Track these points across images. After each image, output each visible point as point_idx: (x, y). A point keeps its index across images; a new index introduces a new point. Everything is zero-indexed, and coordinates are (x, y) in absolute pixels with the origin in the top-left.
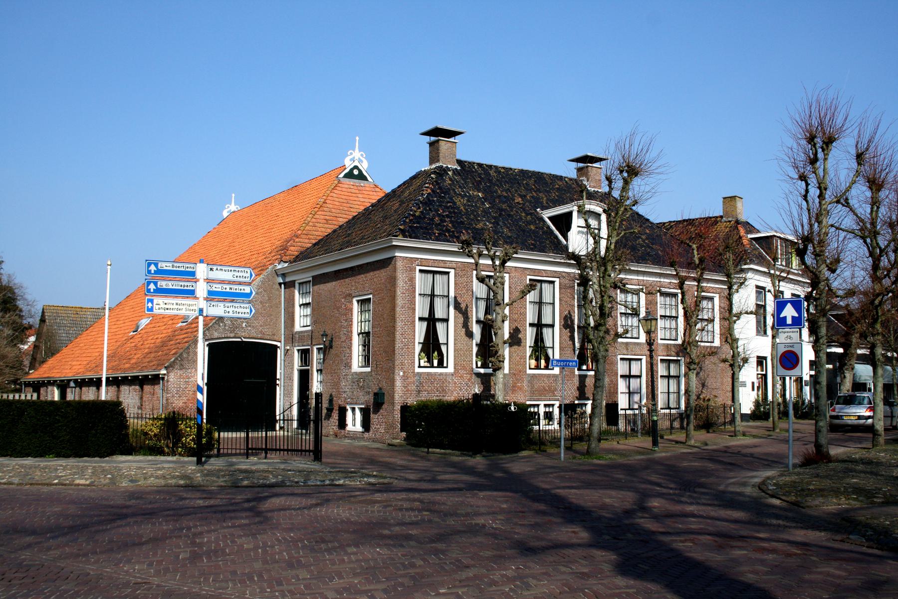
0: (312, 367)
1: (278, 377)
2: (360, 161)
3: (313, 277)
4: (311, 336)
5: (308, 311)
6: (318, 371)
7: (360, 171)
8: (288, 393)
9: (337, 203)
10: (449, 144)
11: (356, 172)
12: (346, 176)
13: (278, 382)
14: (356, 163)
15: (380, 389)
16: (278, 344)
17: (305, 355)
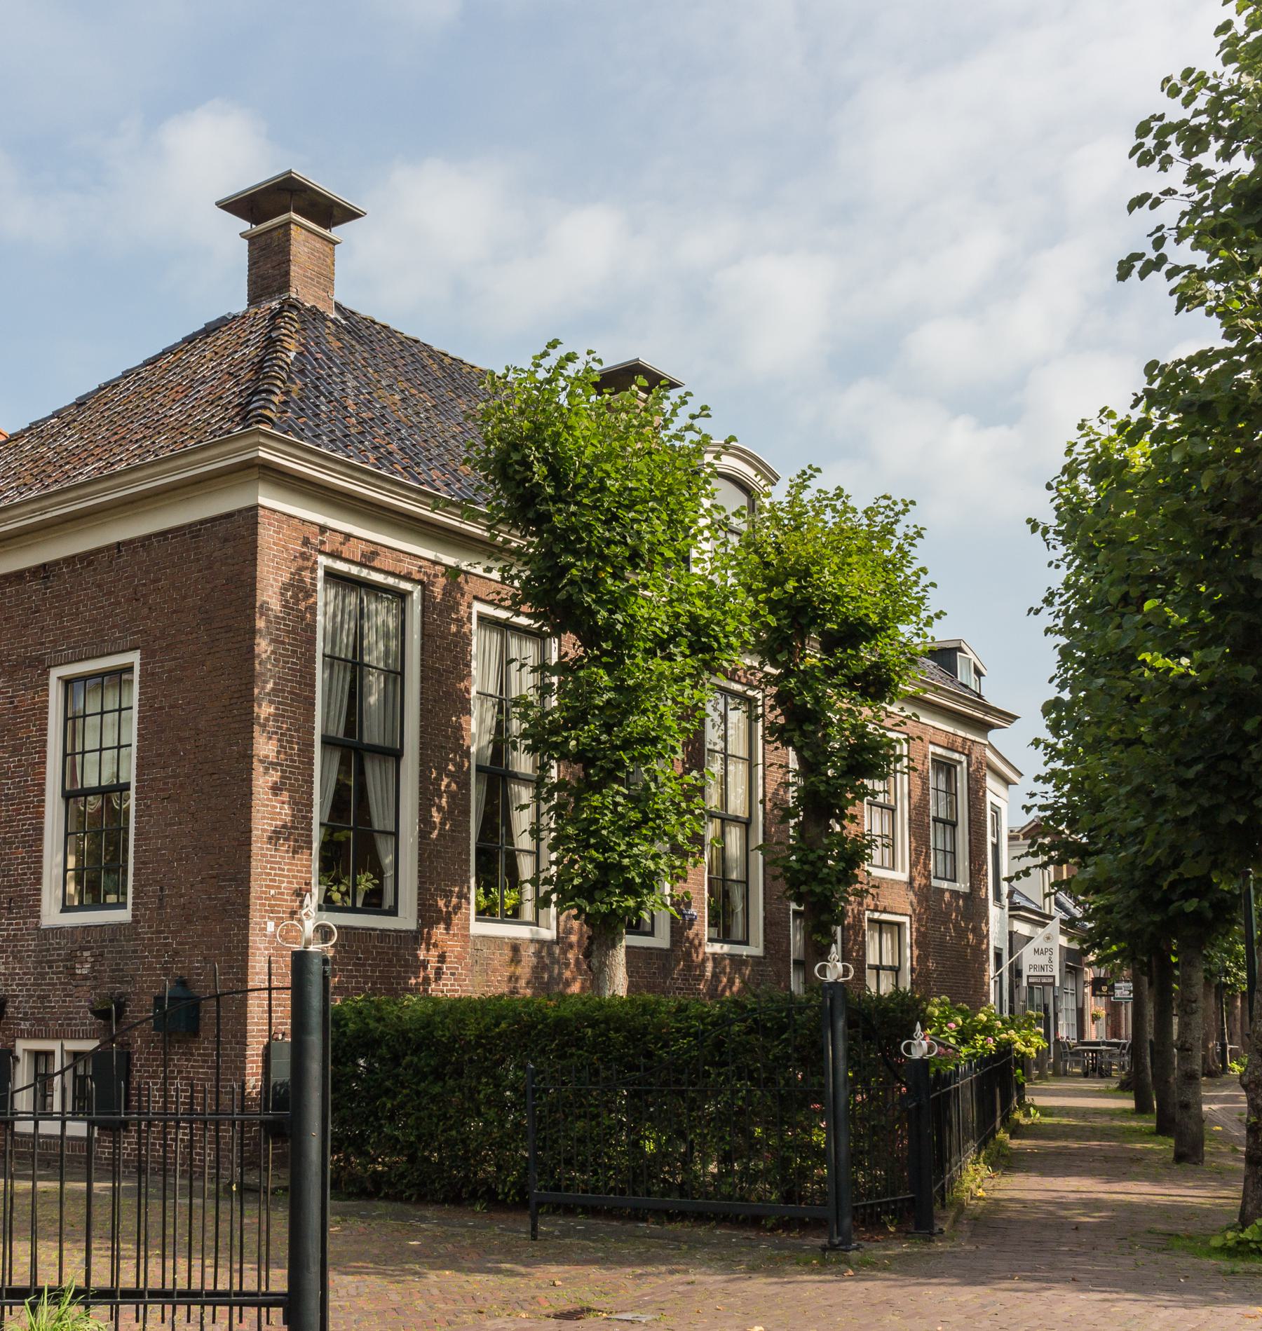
10: (318, 244)
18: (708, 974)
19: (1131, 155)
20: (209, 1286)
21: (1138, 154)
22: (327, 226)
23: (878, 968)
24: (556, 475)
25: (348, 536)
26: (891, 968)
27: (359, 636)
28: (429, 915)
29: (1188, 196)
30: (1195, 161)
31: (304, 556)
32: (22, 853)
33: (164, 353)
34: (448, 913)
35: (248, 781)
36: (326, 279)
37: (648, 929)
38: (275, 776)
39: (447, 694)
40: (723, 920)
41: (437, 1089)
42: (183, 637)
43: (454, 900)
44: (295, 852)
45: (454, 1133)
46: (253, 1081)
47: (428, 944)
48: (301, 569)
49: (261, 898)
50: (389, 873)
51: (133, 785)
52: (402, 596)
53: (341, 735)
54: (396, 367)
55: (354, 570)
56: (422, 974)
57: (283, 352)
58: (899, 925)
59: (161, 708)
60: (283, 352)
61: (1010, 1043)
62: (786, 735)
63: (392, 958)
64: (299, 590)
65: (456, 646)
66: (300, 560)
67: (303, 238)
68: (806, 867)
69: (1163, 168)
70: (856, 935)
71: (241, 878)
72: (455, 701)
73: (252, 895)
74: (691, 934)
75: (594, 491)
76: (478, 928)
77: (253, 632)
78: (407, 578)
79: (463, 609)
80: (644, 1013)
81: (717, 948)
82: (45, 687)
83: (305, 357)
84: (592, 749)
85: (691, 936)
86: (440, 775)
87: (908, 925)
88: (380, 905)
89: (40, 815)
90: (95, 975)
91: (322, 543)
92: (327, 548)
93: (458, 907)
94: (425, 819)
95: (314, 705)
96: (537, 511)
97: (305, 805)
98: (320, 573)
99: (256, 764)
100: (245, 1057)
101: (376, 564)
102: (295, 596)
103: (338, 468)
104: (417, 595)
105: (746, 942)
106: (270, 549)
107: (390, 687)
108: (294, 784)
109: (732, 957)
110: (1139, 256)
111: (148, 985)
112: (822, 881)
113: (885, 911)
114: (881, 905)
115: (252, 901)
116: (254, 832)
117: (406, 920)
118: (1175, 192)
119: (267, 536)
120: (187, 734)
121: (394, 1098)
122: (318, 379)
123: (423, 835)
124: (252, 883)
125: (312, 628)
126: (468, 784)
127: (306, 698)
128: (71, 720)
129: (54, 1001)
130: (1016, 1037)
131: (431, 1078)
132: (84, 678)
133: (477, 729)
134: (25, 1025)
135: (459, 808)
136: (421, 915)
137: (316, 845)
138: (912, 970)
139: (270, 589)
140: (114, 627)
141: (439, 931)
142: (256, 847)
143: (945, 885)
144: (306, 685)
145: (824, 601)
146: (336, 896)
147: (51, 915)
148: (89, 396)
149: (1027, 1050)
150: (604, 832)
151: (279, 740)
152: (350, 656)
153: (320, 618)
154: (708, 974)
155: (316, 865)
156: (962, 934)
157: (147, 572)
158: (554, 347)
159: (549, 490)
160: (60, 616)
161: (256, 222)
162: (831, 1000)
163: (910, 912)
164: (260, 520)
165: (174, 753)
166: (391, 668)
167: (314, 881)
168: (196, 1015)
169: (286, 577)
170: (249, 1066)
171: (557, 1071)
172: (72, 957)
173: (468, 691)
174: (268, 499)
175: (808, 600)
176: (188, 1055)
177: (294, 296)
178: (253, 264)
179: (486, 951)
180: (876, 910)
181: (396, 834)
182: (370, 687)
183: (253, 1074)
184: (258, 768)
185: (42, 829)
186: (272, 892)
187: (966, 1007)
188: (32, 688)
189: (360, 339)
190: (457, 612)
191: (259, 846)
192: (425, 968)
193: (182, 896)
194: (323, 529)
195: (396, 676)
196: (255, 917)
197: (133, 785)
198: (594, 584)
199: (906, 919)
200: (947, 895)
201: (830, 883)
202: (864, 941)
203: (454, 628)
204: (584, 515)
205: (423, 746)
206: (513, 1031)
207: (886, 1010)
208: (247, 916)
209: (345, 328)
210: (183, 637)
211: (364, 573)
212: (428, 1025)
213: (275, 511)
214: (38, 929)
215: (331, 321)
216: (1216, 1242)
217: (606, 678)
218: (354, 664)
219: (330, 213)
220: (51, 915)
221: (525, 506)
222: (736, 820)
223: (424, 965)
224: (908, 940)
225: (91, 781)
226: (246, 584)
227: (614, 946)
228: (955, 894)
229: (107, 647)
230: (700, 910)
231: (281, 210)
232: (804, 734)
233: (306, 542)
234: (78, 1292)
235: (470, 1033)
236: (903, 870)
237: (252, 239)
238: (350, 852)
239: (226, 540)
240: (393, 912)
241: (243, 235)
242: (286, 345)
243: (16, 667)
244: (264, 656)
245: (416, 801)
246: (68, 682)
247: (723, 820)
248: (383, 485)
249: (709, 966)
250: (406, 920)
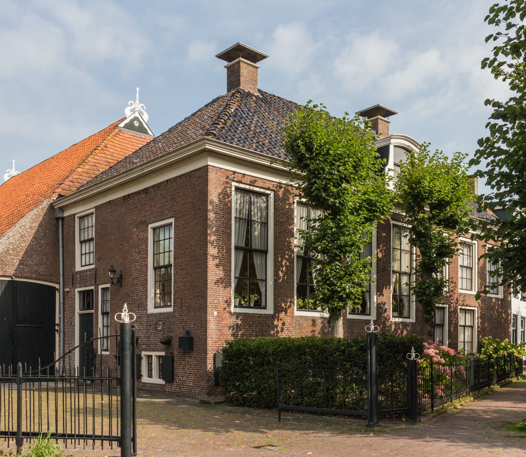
0: (97, 310)
1: (57, 322)
2: (140, 113)
3: (96, 207)
4: (95, 276)
5: (91, 247)
6: (103, 314)
7: (140, 123)
8: (68, 337)
9: (119, 149)
10: (251, 69)
11: (136, 124)
12: (126, 126)
13: (57, 328)
14: (137, 115)
15: (188, 333)
16: (57, 286)
17: (88, 299)
18: (393, 329)
19: (485, 20)
20: (77, 433)
21: (488, 20)
22: (255, 62)
23: (464, 326)
24: (309, 149)
25: (244, 175)
26: (470, 326)
27: (250, 210)
28: (278, 309)
29: (506, 35)
30: (508, 21)
31: (227, 183)
32: (141, 288)
33: (198, 111)
34: (286, 308)
35: (206, 263)
36: (255, 81)
37: (368, 313)
38: (217, 261)
39: (285, 230)
40: (398, 309)
41: (261, 370)
42: (187, 213)
43: (288, 304)
44: (225, 287)
45: (266, 385)
46: (210, 366)
47: (278, 319)
48: (225, 187)
49: (211, 303)
50: (263, 294)
51: (173, 264)
52: (267, 195)
53: (243, 246)
54: (278, 112)
55: (247, 187)
56: (276, 330)
57: (239, 109)
58: (473, 311)
59: (180, 238)
60: (239, 109)
61: (513, 353)
62: (414, 242)
63: (266, 324)
64: (225, 195)
65: (288, 213)
66: (225, 184)
67: (245, 67)
68: (421, 290)
69: (497, 24)
70: (455, 314)
71: (204, 297)
72: (287, 233)
73: (208, 302)
74: (386, 315)
75: (324, 155)
76: (297, 313)
77: (206, 210)
78: (268, 189)
79: (291, 200)
80: (325, 343)
81: (397, 320)
82: (147, 231)
83: (238, 110)
84: (327, 249)
85: (386, 316)
86: (282, 259)
87: (477, 311)
88: (261, 305)
89: (147, 275)
90: (163, 330)
91: (234, 178)
92: (236, 179)
93: (290, 306)
94: (276, 274)
95: (231, 235)
96: (304, 163)
97: (228, 271)
98: (233, 189)
99: (209, 256)
100: (206, 358)
101: (256, 184)
102: (224, 197)
103: (237, 150)
104: (272, 195)
105: (409, 318)
106: (213, 180)
107: (263, 229)
108: (224, 263)
109: (402, 323)
110: (488, 59)
111: (179, 333)
112: (427, 295)
113: (467, 306)
114: (465, 303)
115: (208, 304)
116: (209, 281)
117: (270, 311)
118: (501, 34)
119: (212, 176)
120: (188, 247)
121: (248, 372)
122: (241, 118)
123: (275, 281)
124: (208, 298)
125: (230, 208)
126: (293, 262)
127: (228, 233)
128: (156, 242)
129: (152, 339)
130: (515, 351)
131: (260, 366)
132: (159, 227)
133: (297, 242)
134: (144, 347)
135: (290, 271)
136: (275, 309)
137: (233, 285)
138: (478, 327)
139: (214, 194)
140: (166, 209)
141: (282, 315)
142: (209, 286)
143: (493, 296)
144: (228, 228)
145: (425, 193)
146: (243, 302)
147: (151, 310)
148: (172, 128)
149: (519, 356)
150: (332, 279)
151: (218, 248)
152: (247, 218)
153: (233, 205)
154: (393, 329)
155: (232, 292)
156: (500, 314)
157: (176, 190)
158: (310, 103)
159: (307, 155)
160: (151, 206)
161: (230, 61)
162: (370, 339)
163: (477, 305)
164: (209, 170)
165: (185, 253)
166: (263, 221)
167: (233, 298)
168: (191, 343)
169: (220, 190)
170: (208, 361)
171: (298, 364)
172: (156, 324)
173: (293, 229)
174: (212, 162)
175: (419, 193)
176: (190, 357)
177: (241, 88)
178: (229, 77)
179: (301, 321)
180: (463, 305)
181: (266, 280)
182: (255, 229)
183: (210, 364)
184: (210, 258)
185: (147, 280)
186: (216, 301)
187: (498, 340)
188: (143, 231)
189: (266, 102)
190: (289, 201)
191: (211, 285)
192: (277, 328)
193: (187, 303)
194: (234, 173)
195: (265, 224)
196: (209, 310)
197: (173, 264)
198: (326, 189)
199: (476, 309)
200: (494, 300)
201: (430, 296)
202: (458, 317)
203: (287, 207)
204: (321, 164)
205: (275, 249)
206: (285, 350)
207: (404, 342)
208: (206, 309)
209: (260, 99)
210: (187, 213)
211: (252, 188)
212: (258, 347)
213: (215, 167)
214: (147, 314)
215: (256, 96)
216: (518, 426)
217: (331, 223)
218: (248, 221)
219: (255, 57)
220: (151, 310)
221: (300, 161)
222: (405, 273)
223: (276, 326)
224: (477, 316)
225: (162, 264)
226: (204, 193)
227: (338, 320)
228: (497, 299)
229: (165, 217)
230: (389, 306)
231: (237, 56)
232: (421, 242)
233: (227, 177)
234: (53, 435)
235: (270, 351)
236: (475, 291)
237: (228, 68)
238: (248, 286)
239: (199, 178)
240: (265, 308)
241: (225, 67)
242: (231, 106)
243: (139, 224)
244: (212, 219)
245: (273, 269)
246: (154, 229)
247: (400, 274)
248: (255, 156)
249: (393, 326)
250: (270, 311)
